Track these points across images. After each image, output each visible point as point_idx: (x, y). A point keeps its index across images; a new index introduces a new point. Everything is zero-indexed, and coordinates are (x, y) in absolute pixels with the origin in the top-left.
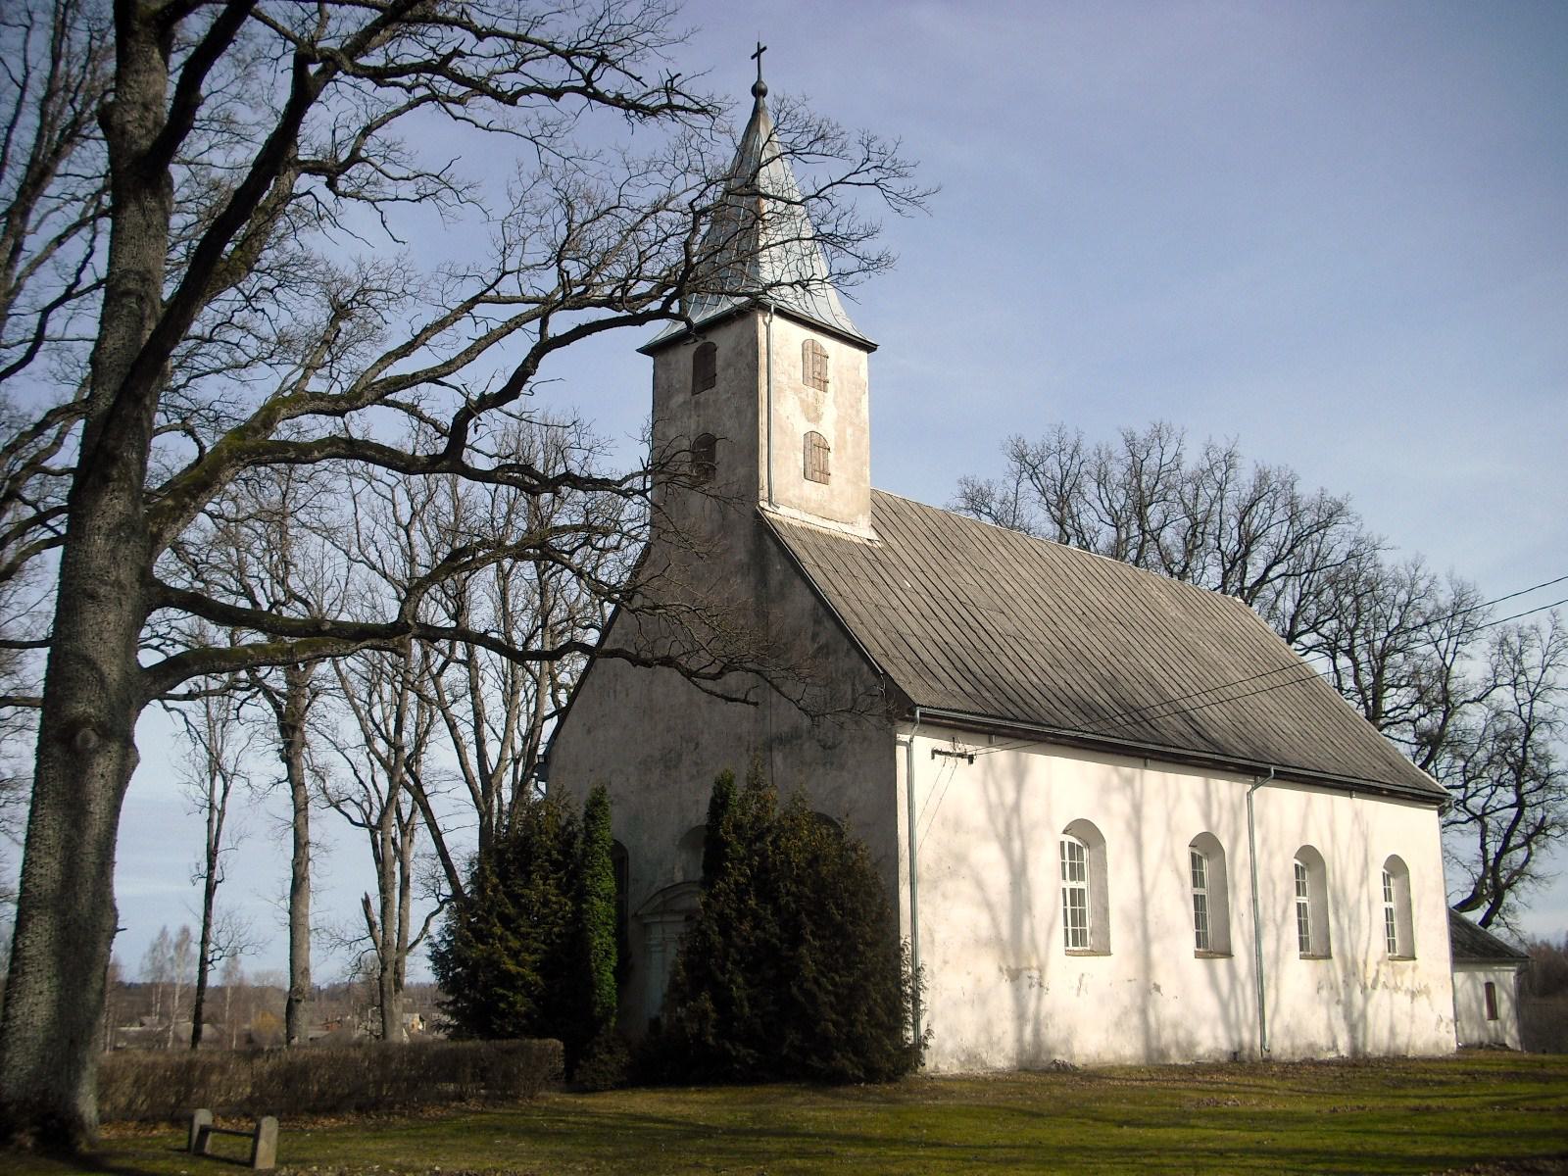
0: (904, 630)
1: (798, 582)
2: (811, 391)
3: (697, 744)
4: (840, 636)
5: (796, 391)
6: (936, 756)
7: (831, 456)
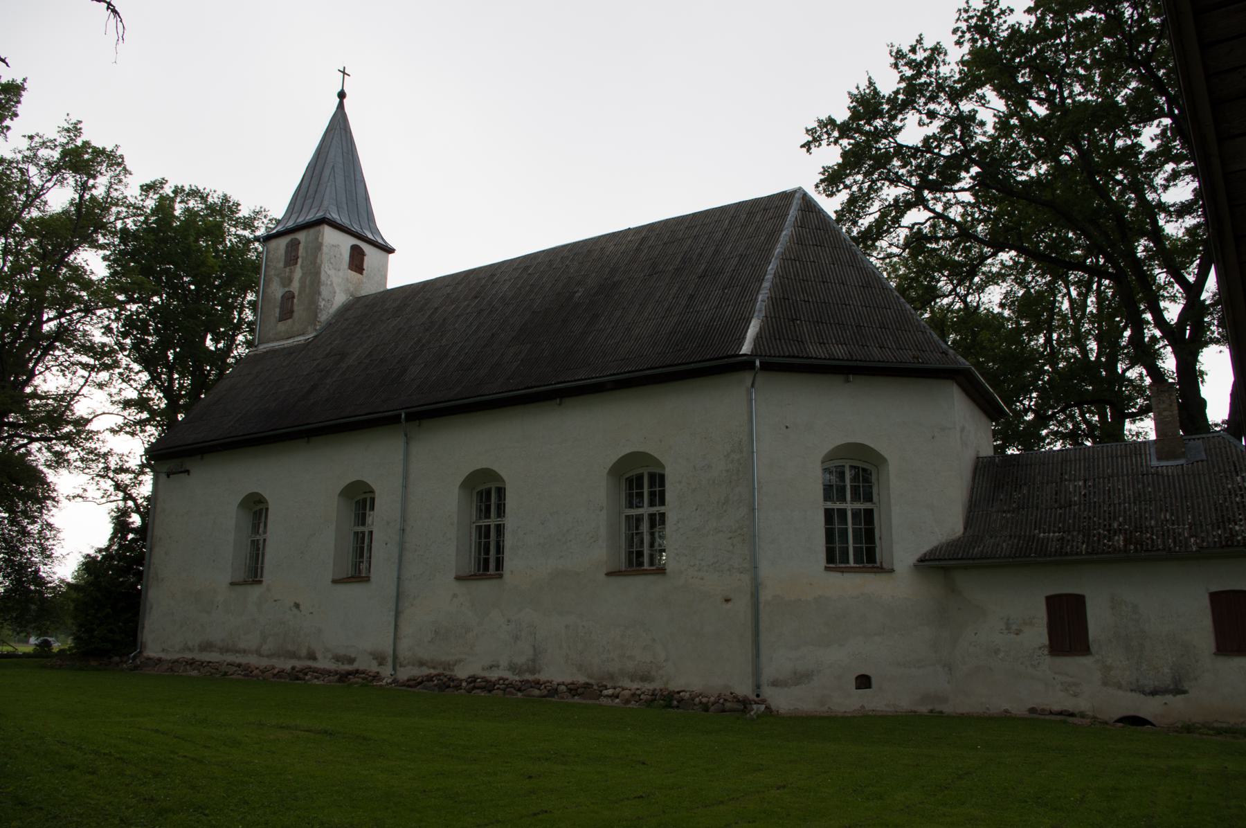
7: (295, 301)
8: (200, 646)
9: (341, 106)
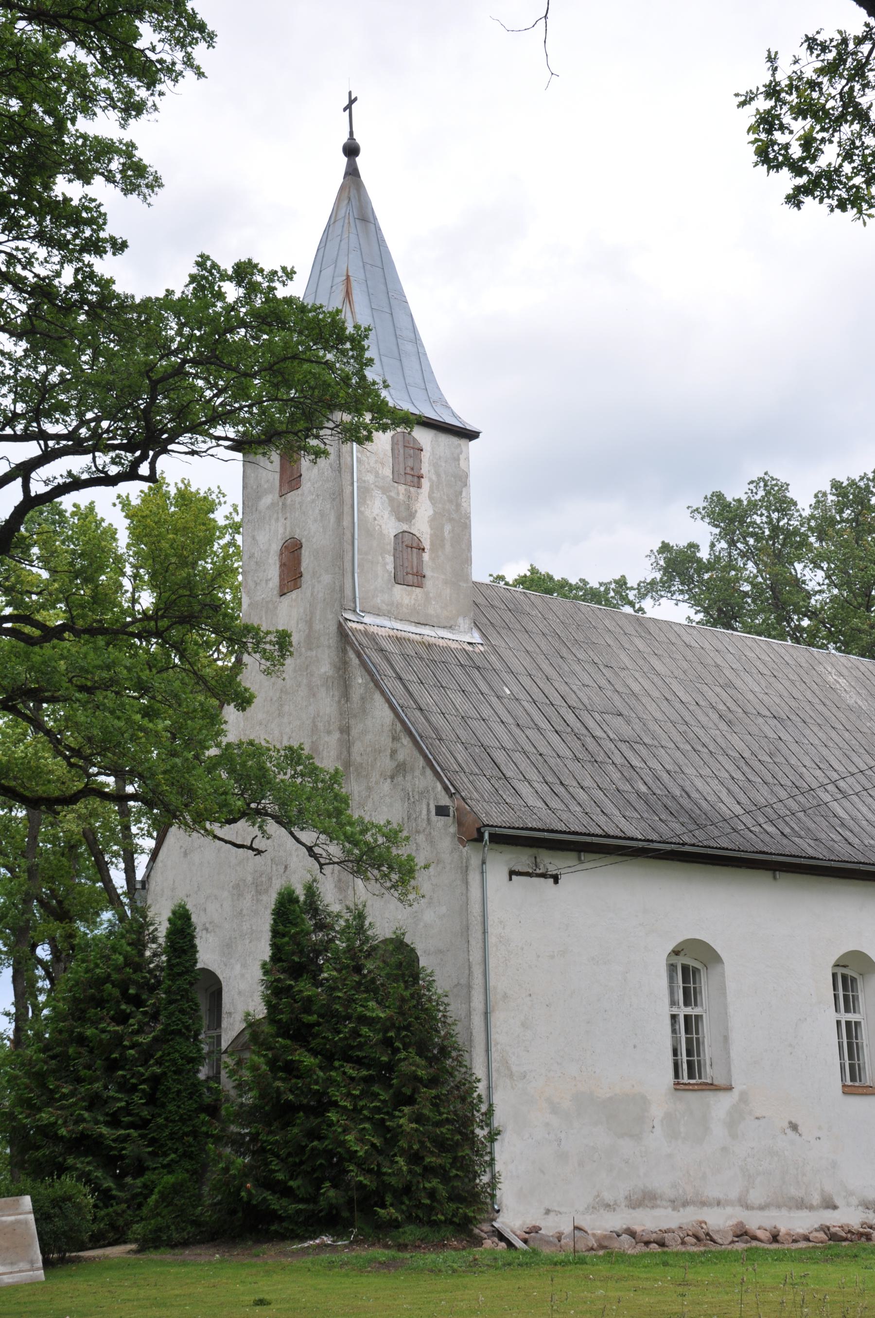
0: (489, 741)
1: (378, 696)
2: (402, 488)
3: (286, 867)
4: (416, 754)
5: (385, 490)
6: (514, 877)
7: (426, 556)
8: (628, 1198)
9: (352, 172)
